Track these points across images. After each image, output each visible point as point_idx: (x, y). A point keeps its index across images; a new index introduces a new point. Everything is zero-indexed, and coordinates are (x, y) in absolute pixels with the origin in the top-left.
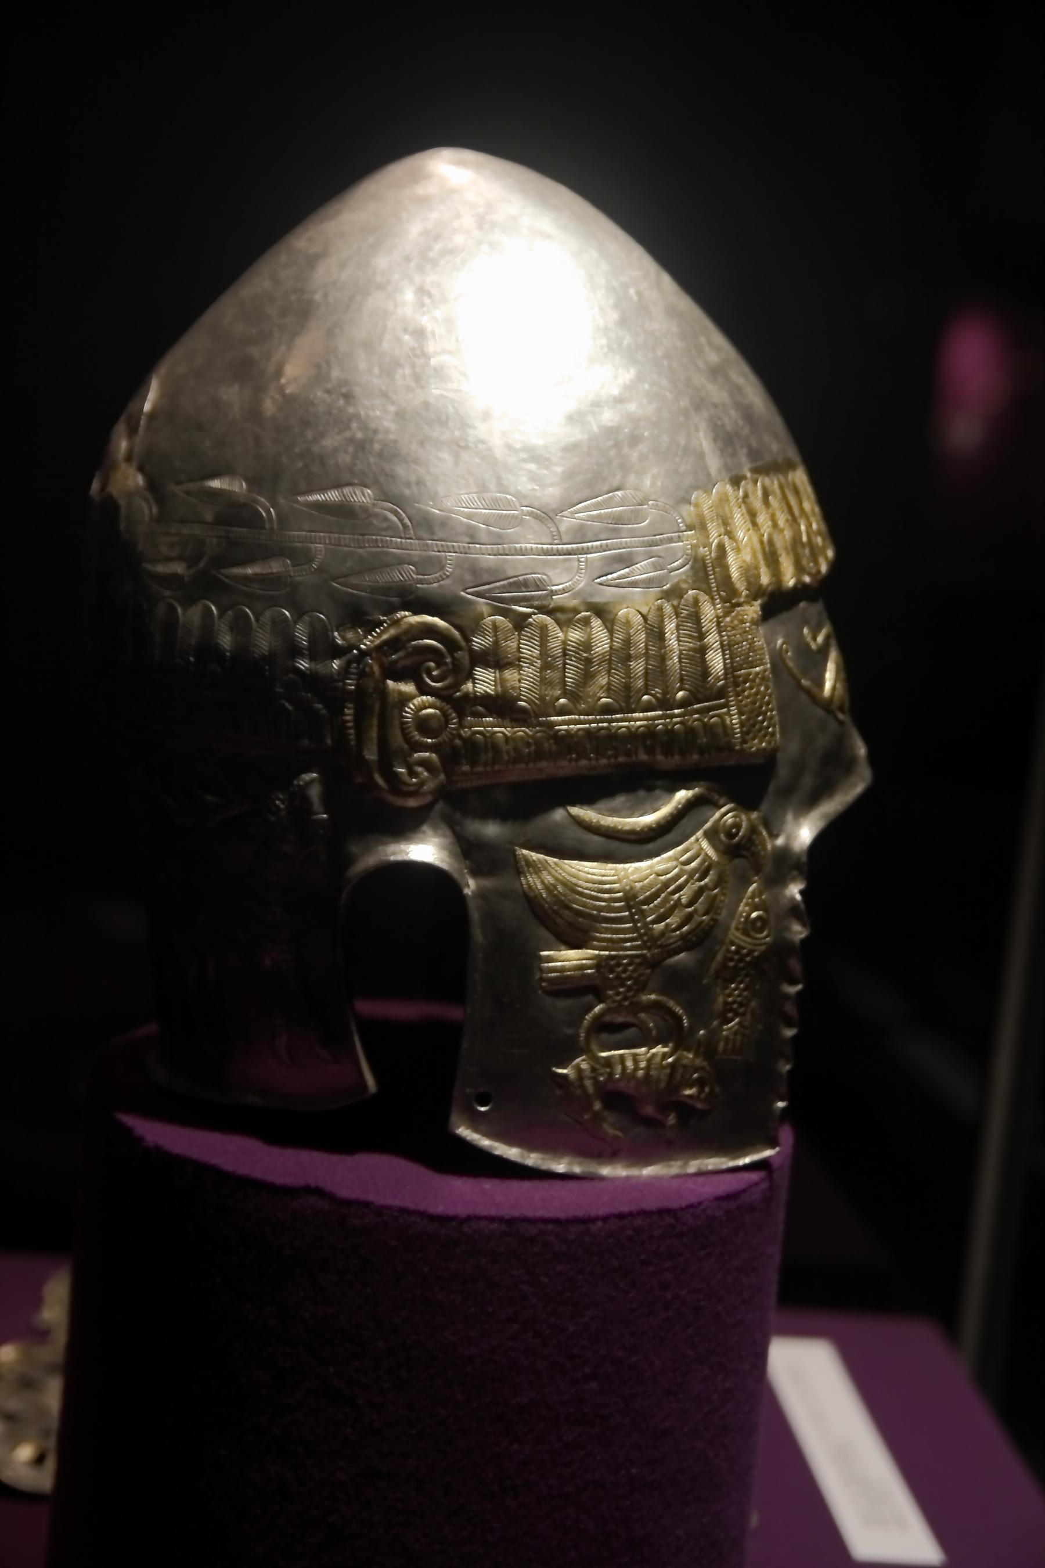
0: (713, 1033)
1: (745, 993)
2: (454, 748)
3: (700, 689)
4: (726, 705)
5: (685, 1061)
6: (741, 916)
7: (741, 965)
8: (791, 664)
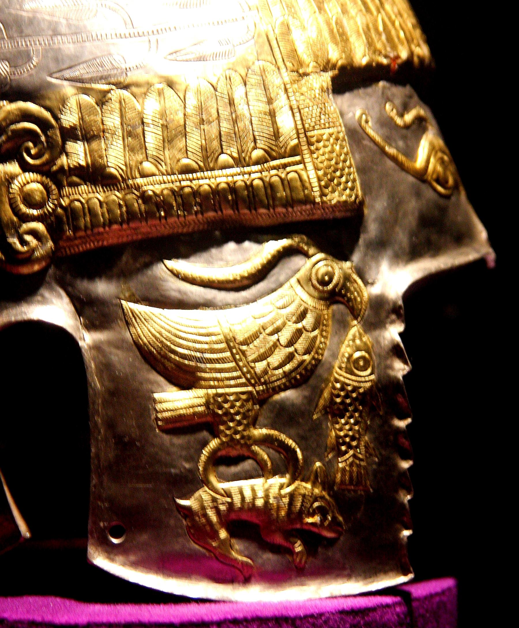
0: (329, 465)
1: (357, 428)
2: (58, 217)
3: (274, 147)
4: (302, 162)
5: (302, 491)
6: (343, 356)
7: (348, 401)
8: (371, 132)
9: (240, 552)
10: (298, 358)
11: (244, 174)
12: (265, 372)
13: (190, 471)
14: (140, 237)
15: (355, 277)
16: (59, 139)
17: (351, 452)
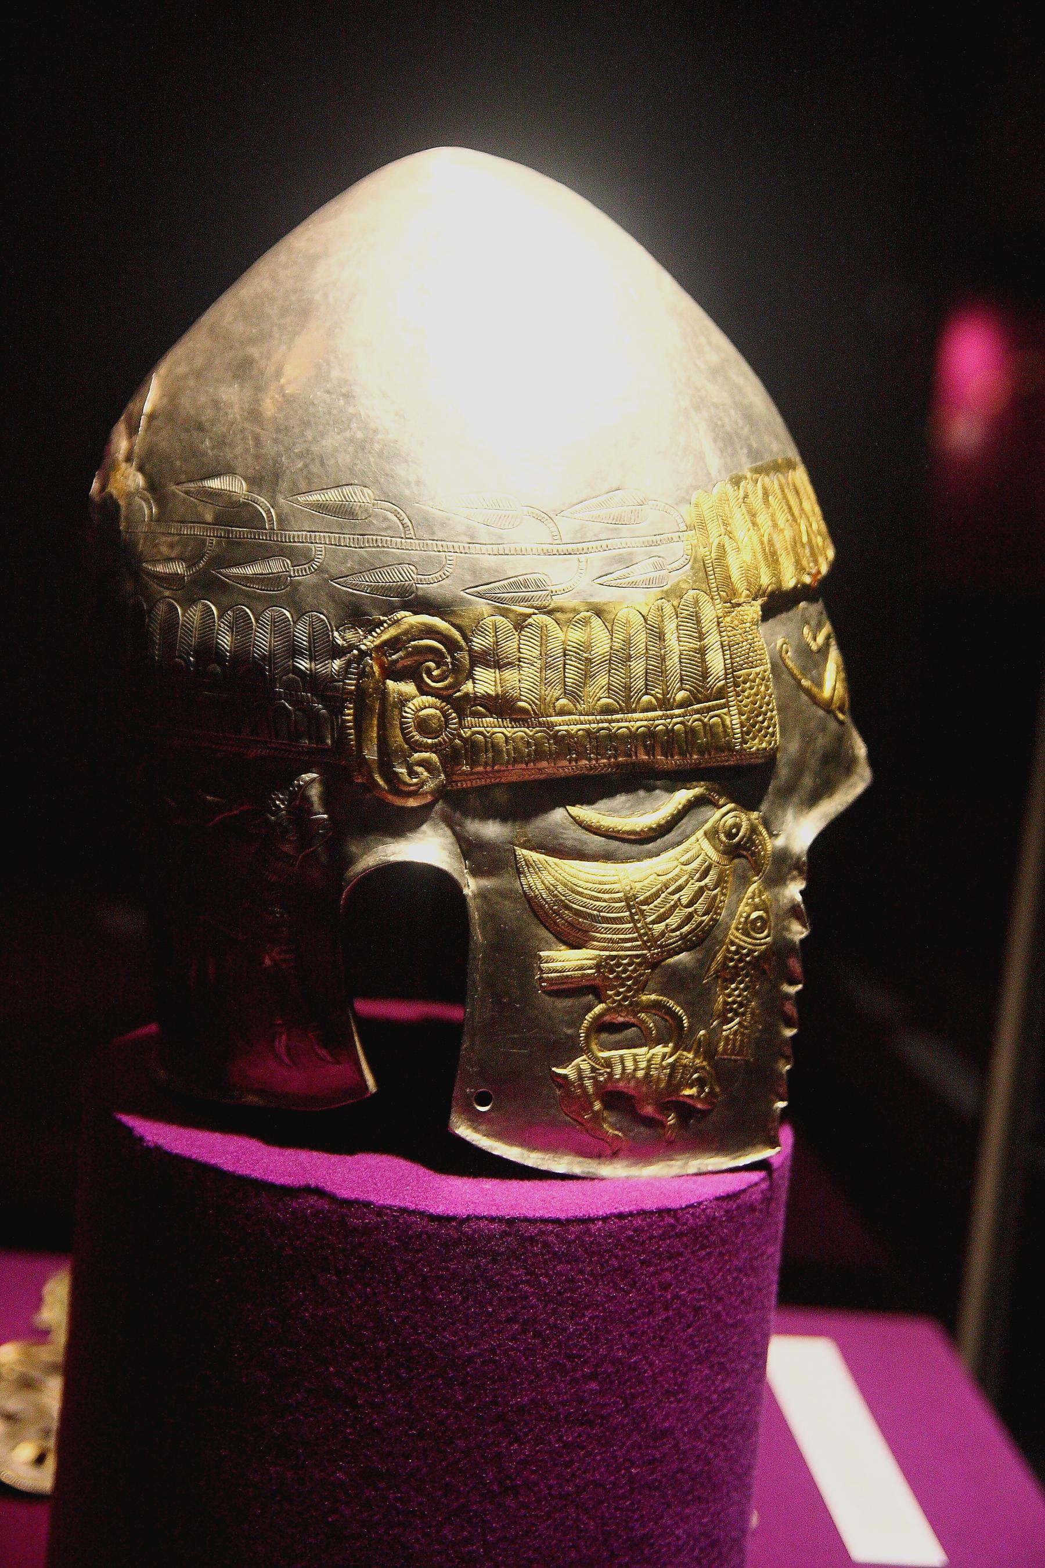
0: (714, 1033)
2: (455, 749)
4: (726, 706)
5: (685, 1061)
8: (791, 664)
9: (613, 1126)
10: (697, 918)
11: (667, 717)
12: (663, 934)
13: (568, 1036)
14: (542, 777)
15: (762, 829)
16: (467, 662)
17: (737, 1020)
